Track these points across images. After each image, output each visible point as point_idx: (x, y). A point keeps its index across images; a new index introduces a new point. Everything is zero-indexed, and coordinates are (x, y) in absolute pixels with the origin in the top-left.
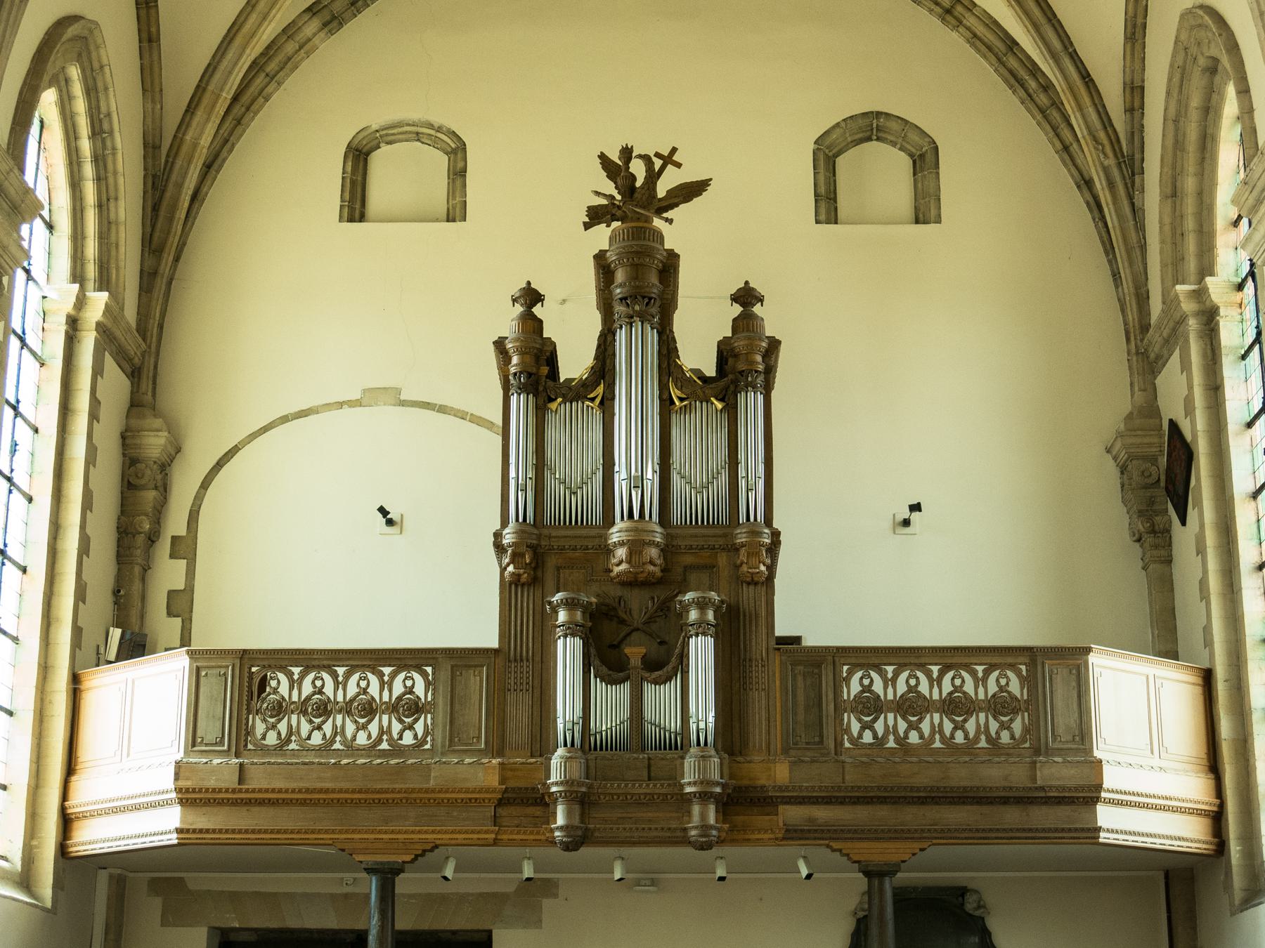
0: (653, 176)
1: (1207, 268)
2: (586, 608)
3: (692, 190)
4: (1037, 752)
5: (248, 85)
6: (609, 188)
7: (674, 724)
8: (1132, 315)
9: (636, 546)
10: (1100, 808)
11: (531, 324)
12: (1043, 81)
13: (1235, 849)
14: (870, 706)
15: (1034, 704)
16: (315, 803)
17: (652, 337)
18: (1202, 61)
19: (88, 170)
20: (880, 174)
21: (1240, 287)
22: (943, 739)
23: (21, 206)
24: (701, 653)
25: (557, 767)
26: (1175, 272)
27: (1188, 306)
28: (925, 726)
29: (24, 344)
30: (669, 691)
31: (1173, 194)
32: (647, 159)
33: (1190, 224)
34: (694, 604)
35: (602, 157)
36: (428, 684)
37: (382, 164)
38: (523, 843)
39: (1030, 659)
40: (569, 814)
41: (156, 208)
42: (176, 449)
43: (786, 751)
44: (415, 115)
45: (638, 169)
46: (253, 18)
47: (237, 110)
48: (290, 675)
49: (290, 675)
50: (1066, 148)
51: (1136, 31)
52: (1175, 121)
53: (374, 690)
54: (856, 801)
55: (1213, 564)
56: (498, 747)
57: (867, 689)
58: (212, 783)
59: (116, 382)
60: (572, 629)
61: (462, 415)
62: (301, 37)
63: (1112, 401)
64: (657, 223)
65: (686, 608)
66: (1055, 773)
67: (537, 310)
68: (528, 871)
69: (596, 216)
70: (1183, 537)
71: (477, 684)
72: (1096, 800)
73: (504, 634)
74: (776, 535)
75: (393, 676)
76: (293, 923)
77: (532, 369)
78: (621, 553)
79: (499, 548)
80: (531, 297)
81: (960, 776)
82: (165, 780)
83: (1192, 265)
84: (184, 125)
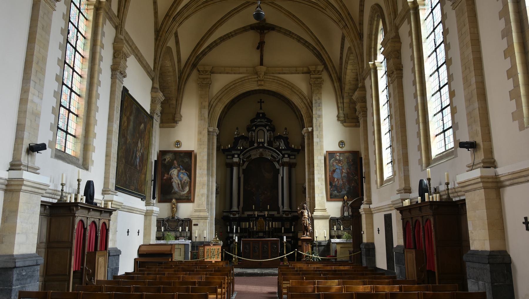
1: (375, 59)
51: (362, 11)
84: (162, 24)
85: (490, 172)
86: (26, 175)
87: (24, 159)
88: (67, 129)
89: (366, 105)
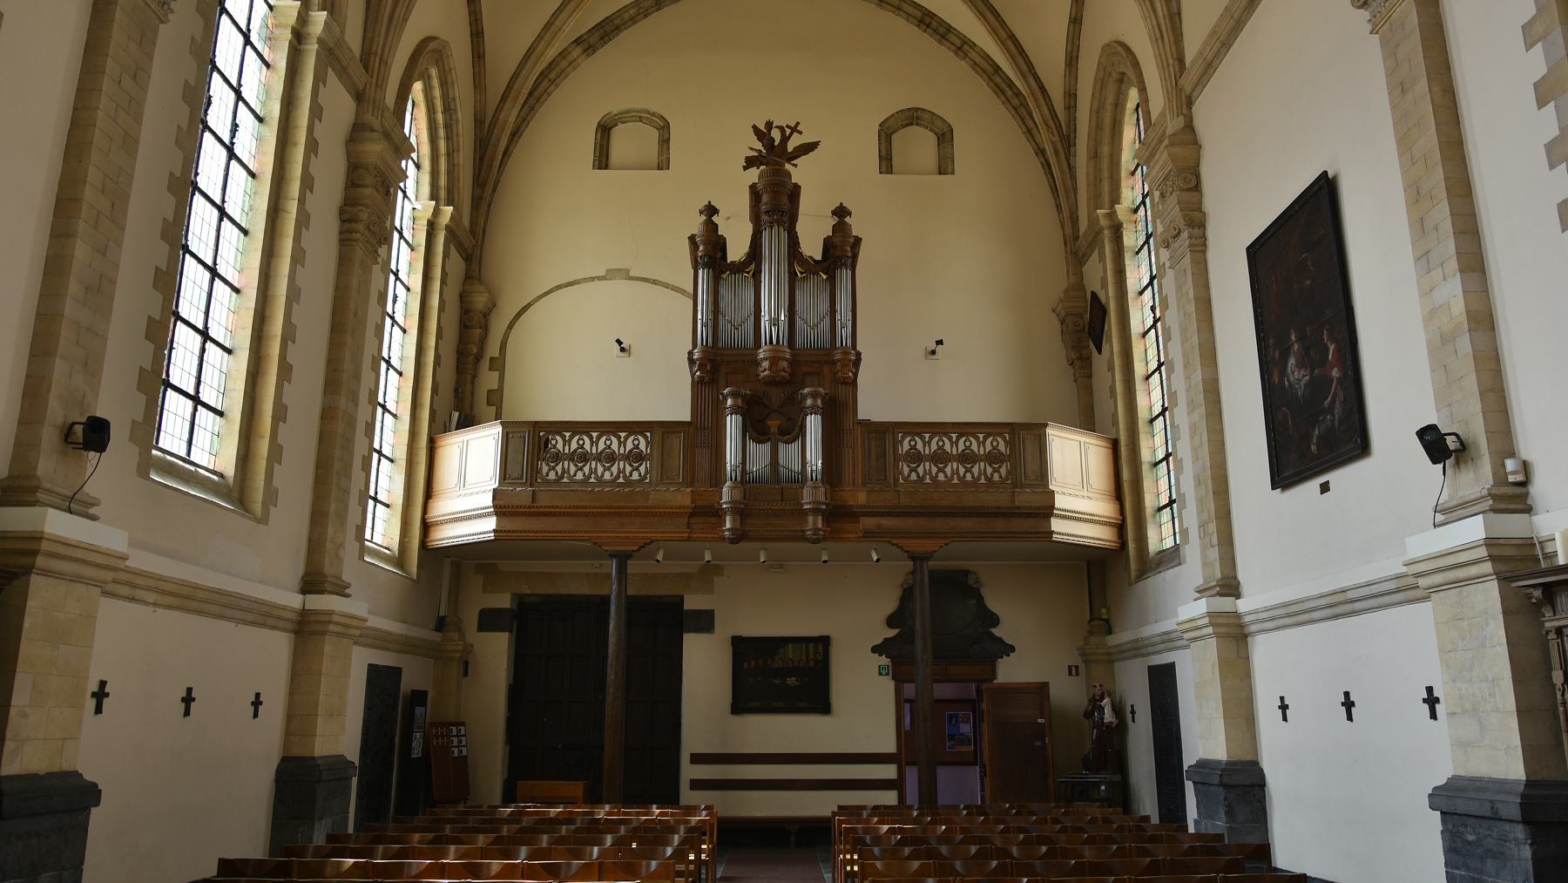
0: (785, 139)
1: (1115, 199)
2: (744, 397)
3: (809, 148)
4: (1015, 485)
5: (538, 86)
6: (759, 146)
7: (797, 467)
8: (1069, 230)
9: (774, 360)
10: (1053, 520)
11: (711, 227)
12: (1018, 91)
13: (1131, 546)
14: (915, 457)
15: (1014, 457)
16: (578, 515)
17: (784, 235)
18: (1115, 75)
19: (442, 133)
20: (918, 145)
21: (1136, 211)
22: (986, 478)
23: (403, 148)
24: (813, 424)
25: (726, 494)
26: (1096, 201)
27: (1104, 222)
28: (948, 470)
29: (397, 278)
30: (795, 447)
31: (1095, 156)
32: (781, 128)
33: (1106, 174)
34: (809, 395)
35: (755, 128)
36: (647, 443)
37: (619, 136)
38: (705, 540)
39: (1010, 430)
40: (733, 521)
41: (481, 159)
42: (492, 306)
43: (864, 484)
44: (639, 106)
45: (776, 135)
46: (542, 44)
47: (532, 101)
48: (563, 437)
49: (563, 437)
50: (1029, 131)
51: (1072, 61)
52: (1097, 112)
53: (615, 446)
54: (898, 515)
55: (1118, 377)
56: (690, 481)
57: (914, 447)
58: (516, 502)
59: (457, 260)
60: (735, 410)
61: (666, 286)
62: (570, 58)
63: (1056, 281)
64: (787, 166)
65: (804, 398)
66: (1026, 499)
67: (715, 218)
68: (708, 557)
69: (750, 163)
70: (1099, 362)
71: (677, 442)
72: (1051, 515)
73: (693, 413)
74: (859, 354)
75: (626, 438)
76: (563, 590)
77: (709, 251)
78: (766, 364)
79: (691, 361)
80: (711, 210)
81: (969, 500)
82: (488, 500)
83: (1106, 198)
84: (499, 109)
85: (1512, 526)
86: (57, 524)
87: (48, 466)
88: (197, 391)
89: (1200, 202)
